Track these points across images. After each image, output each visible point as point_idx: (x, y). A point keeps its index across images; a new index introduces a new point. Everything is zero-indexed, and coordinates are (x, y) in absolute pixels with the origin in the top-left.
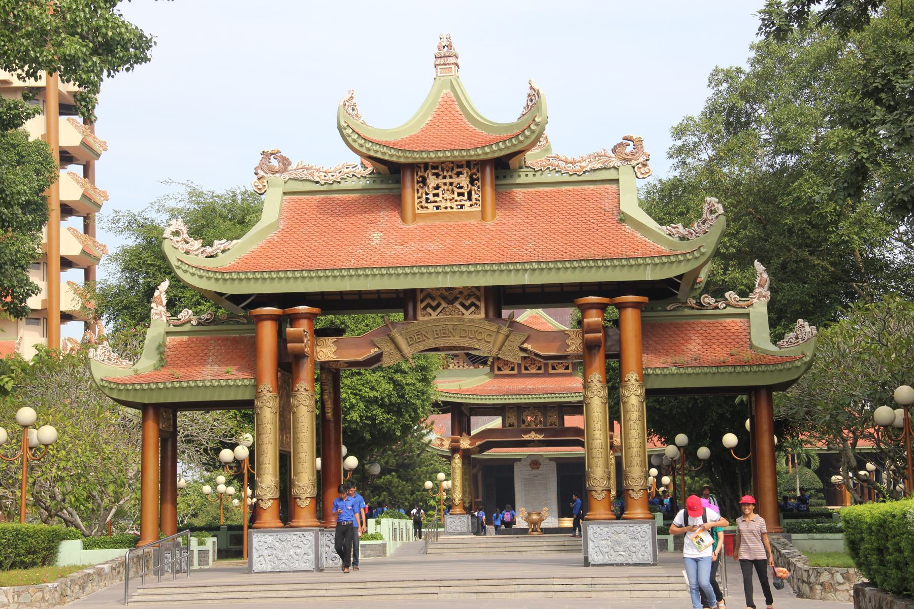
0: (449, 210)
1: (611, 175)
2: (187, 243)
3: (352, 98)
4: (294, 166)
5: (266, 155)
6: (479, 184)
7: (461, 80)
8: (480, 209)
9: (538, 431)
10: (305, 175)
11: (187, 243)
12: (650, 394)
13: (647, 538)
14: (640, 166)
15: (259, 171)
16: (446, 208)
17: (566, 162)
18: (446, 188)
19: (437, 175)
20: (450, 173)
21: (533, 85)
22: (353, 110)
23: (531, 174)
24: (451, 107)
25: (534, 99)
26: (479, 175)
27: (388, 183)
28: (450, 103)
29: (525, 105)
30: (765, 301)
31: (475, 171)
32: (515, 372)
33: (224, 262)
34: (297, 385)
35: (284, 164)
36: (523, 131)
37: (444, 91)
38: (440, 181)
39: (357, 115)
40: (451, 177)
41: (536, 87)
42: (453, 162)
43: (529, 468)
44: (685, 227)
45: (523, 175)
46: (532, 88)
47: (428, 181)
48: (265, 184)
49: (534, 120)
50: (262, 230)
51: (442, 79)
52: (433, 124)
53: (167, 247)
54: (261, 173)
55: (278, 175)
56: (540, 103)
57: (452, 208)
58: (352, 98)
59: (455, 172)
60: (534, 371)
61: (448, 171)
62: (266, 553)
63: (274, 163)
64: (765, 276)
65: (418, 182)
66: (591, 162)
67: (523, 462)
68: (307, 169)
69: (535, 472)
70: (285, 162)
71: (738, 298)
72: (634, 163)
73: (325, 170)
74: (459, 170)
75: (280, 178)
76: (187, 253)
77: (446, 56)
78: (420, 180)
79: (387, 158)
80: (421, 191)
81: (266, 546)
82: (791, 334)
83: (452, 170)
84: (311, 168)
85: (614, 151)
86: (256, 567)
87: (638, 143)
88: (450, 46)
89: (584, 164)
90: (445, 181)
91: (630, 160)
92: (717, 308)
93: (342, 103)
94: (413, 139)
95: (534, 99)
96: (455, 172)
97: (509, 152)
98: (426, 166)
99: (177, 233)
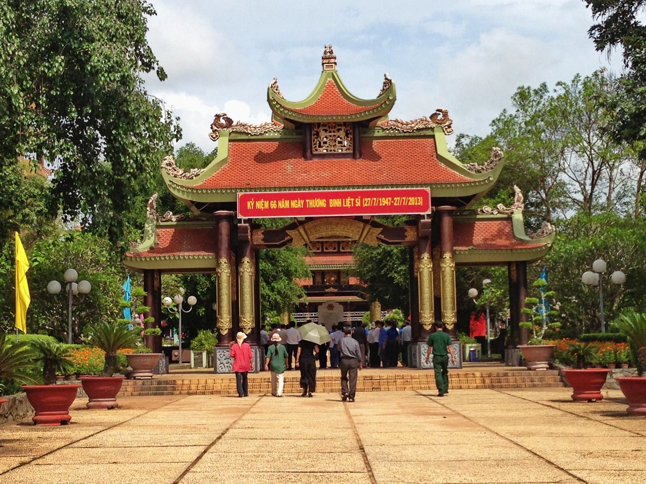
0: (333, 152)
1: (429, 133)
2: (175, 170)
3: (276, 82)
4: (234, 123)
5: (218, 117)
6: (352, 136)
7: (338, 73)
8: (352, 152)
9: (334, 287)
10: (242, 129)
11: (175, 170)
12: (458, 265)
13: (456, 353)
14: (446, 127)
15: (214, 126)
16: (331, 151)
17: (402, 124)
18: (331, 138)
19: (326, 131)
20: (333, 129)
21: (387, 77)
22: (277, 90)
23: (381, 131)
24: (333, 88)
25: (388, 83)
26: (351, 131)
27: (293, 135)
28: (332, 86)
29: (382, 89)
30: (521, 210)
31: (349, 128)
32: (320, 251)
33: (197, 183)
34: (221, 260)
35: (228, 122)
36: (382, 105)
37: (329, 79)
38: (328, 134)
39: (279, 93)
40: (334, 132)
41: (389, 78)
42: (335, 123)
43: (327, 309)
44: (479, 165)
45: (376, 131)
46: (386, 79)
47: (320, 134)
48: (217, 134)
49: (388, 98)
50: (217, 164)
51: (327, 72)
52: (322, 100)
53: (164, 172)
54: (215, 128)
55: (225, 129)
56: (392, 87)
57: (334, 151)
58: (276, 82)
59: (336, 129)
60: (331, 250)
61: (332, 128)
62: (225, 362)
63: (223, 121)
64: (521, 195)
65: (314, 135)
66: (417, 124)
67: (324, 305)
68: (243, 126)
69: (330, 311)
70: (229, 121)
71: (505, 208)
72: (443, 125)
73: (254, 126)
74: (340, 128)
75: (227, 131)
76: (175, 176)
77: (329, 58)
78: (315, 133)
79: (296, 119)
80: (316, 140)
81: (224, 357)
82: (539, 230)
83: (335, 127)
84: (246, 125)
85: (431, 117)
86: (219, 370)
87: (445, 114)
88: (331, 52)
89: (413, 125)
90: (330, 134)
91: (441, 124)
92: (492, 214)
93: (270, 86)
94: (311, 108)
95: (388, 83)
96: (336, 129)
97: (368, 118)
98: (319, 125)
99: (170, 165)
